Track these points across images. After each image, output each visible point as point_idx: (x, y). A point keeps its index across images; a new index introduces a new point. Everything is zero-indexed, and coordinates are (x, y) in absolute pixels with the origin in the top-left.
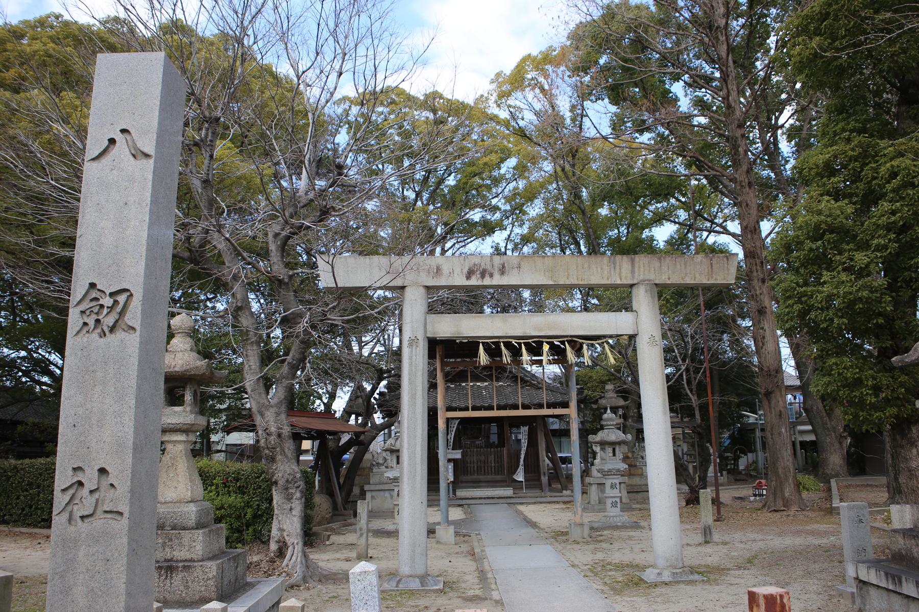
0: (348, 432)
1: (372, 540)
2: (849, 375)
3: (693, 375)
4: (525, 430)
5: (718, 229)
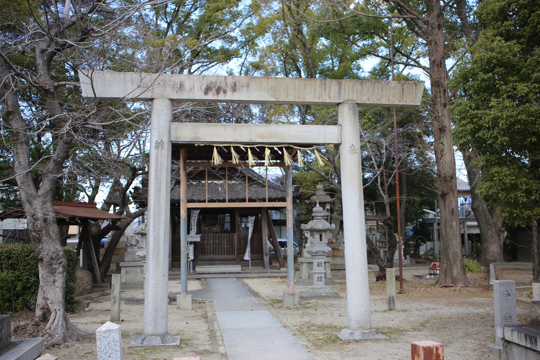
0: (107, 219)
1: (124, 306)
2: (508, 181)
3: (385, 179)
4: (252, 219)
5: (412, 63)
